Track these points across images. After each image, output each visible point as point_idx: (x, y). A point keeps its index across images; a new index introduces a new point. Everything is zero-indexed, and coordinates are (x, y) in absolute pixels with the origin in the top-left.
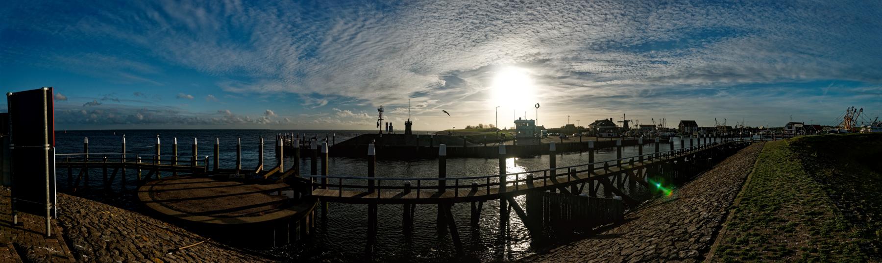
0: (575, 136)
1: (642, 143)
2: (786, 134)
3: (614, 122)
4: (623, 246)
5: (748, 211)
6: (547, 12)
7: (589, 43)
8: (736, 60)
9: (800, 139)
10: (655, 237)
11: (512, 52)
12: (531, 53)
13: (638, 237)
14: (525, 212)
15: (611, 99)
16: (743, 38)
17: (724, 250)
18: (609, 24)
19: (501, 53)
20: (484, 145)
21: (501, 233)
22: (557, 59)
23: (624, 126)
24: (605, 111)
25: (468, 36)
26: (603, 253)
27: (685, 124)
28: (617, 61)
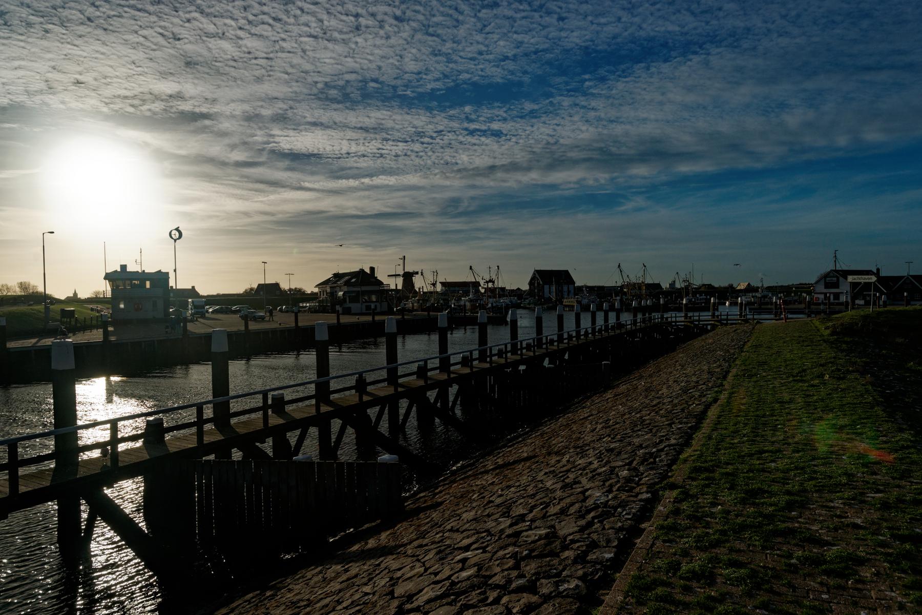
2: (819, 304)
3: (381, 276)
4: (399, 574)
5: (709, 499)
7: (316, 82)
9: (865, 317)
10: (477, 549)
11: (96, 79)
13: (434, 552)
14: (142, 525)
15: (372, 220)
16: (690, 60)
17: (649, 588)
18: (366, 40)
22: (233, 116)
26: (352, 595)
27: (543, 278)
28: (386, 130)
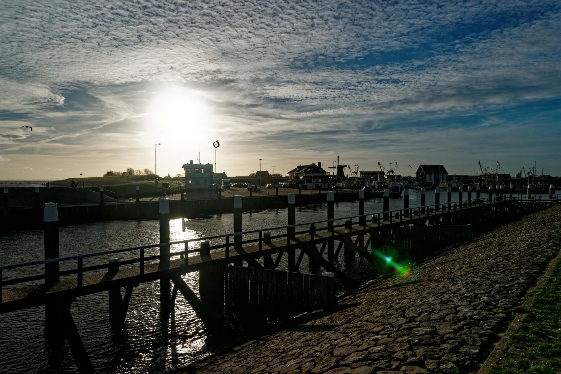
0: (270, 187)
1: (363, 197)
3: (325, 167)
4: (336, 342)
6: (232, 14)
7: (289, 58)
8: (518, 63)
10: (384, 334)
11: (180, 66)
12: (207, 70)
13: (357, 332)
14: (198, 296)
16: (534, 24)
18: (317, 32)
19: (163, 65)
20: (135, 200)
21: (162, 329)
22: (245, 80)
23: (337, 173)
24: (311, 153)
25: (106, 29)
26: (308, 351)
27: (425, 170)
28: (328, 83)
